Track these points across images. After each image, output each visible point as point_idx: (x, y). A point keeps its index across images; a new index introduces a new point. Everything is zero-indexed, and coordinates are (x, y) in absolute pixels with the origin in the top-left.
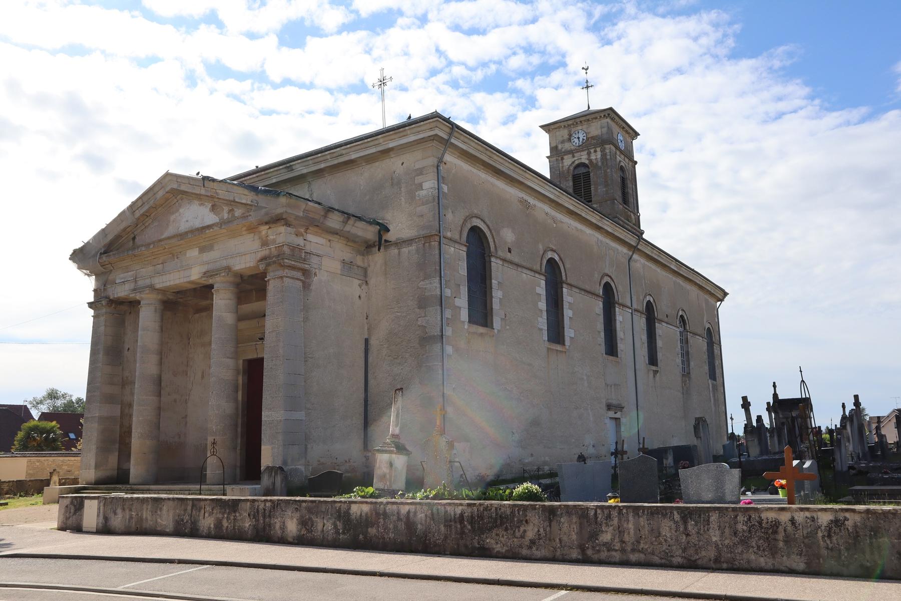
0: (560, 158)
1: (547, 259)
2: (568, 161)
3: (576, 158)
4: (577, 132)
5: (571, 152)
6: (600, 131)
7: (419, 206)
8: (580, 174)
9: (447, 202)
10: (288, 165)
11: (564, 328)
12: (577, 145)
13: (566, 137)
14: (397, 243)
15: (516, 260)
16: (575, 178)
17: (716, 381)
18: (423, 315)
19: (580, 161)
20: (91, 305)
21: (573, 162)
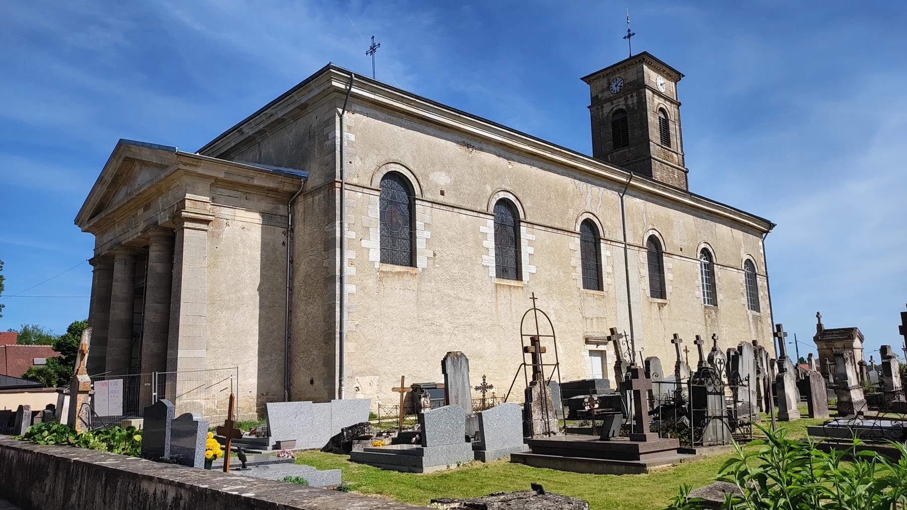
0: (600, 107)
1: (497, 199)
2: (607, 108)
3: (614, 106)
4: (615, 80)
5: (610, 100)
6: (636, 76)
7: (326, 156)
8: (619, 120)
9: (354, 150)
10: (239, 129)
11: (521, 264)
12: (616, 92)
13: (606, 86)
14: (311, 192)
15: (452, 202)
16: (615, 124)
17: (759, 311)
18: (327, 257)
19: (618, 107)
20: (91, 261)
21: (612, 110)
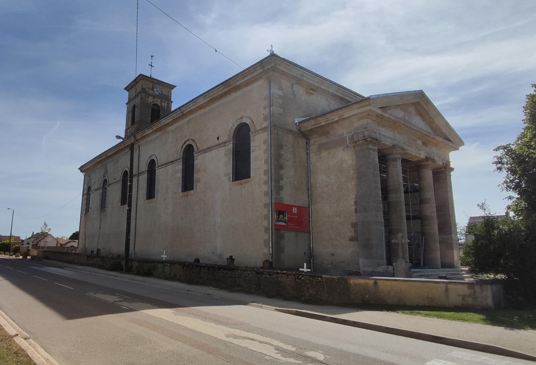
5: (154, 97)
19: (156, 103)
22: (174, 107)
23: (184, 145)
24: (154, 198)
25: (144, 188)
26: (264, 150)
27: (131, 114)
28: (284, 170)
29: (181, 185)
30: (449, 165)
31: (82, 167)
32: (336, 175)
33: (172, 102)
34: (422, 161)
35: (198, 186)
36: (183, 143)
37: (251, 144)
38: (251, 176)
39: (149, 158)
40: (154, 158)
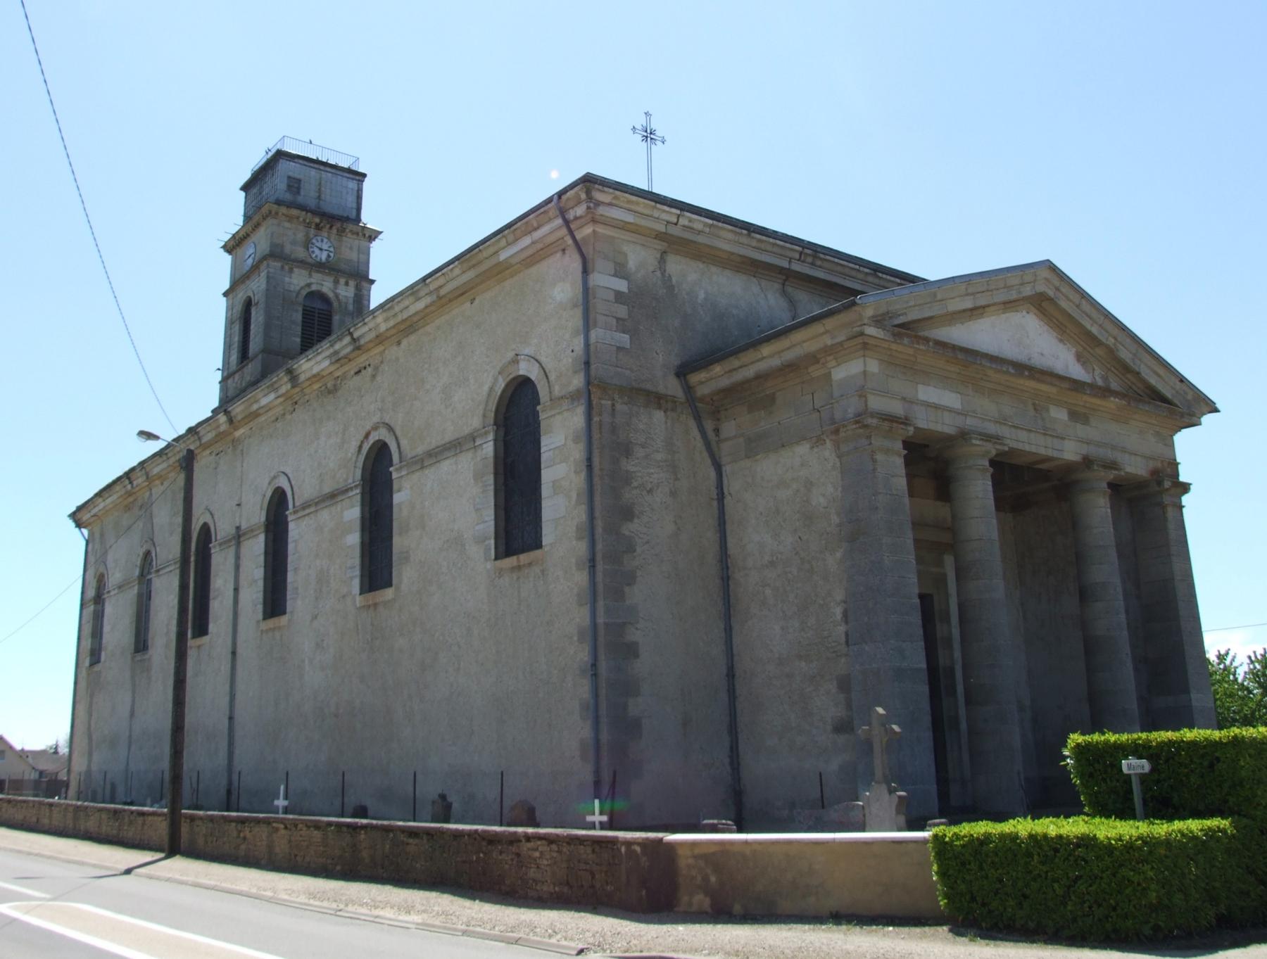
21: (309, 285)
22: (377, 296)
23: (366, 444)
24: (390, 585)
25: (256, 581)
26: (575, 459)
27: (237, 328)
28: (636, 520)
29: (357, 572)
30: (1176, 474)
31: (79, 509)
32: (796, 530)
33: (372, 282)
34: (1070, 468)
35: (405, 576)
36: (362, 438)
37: (542, 444)
38: (543, 544)
39: (270, 483)
40: (283, 483)
